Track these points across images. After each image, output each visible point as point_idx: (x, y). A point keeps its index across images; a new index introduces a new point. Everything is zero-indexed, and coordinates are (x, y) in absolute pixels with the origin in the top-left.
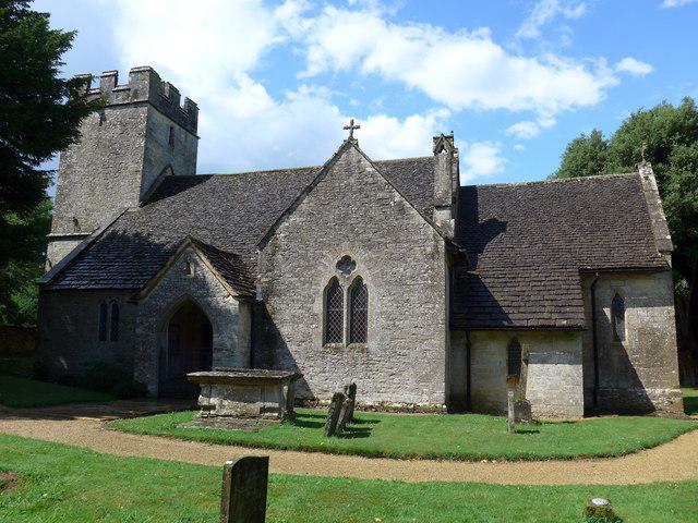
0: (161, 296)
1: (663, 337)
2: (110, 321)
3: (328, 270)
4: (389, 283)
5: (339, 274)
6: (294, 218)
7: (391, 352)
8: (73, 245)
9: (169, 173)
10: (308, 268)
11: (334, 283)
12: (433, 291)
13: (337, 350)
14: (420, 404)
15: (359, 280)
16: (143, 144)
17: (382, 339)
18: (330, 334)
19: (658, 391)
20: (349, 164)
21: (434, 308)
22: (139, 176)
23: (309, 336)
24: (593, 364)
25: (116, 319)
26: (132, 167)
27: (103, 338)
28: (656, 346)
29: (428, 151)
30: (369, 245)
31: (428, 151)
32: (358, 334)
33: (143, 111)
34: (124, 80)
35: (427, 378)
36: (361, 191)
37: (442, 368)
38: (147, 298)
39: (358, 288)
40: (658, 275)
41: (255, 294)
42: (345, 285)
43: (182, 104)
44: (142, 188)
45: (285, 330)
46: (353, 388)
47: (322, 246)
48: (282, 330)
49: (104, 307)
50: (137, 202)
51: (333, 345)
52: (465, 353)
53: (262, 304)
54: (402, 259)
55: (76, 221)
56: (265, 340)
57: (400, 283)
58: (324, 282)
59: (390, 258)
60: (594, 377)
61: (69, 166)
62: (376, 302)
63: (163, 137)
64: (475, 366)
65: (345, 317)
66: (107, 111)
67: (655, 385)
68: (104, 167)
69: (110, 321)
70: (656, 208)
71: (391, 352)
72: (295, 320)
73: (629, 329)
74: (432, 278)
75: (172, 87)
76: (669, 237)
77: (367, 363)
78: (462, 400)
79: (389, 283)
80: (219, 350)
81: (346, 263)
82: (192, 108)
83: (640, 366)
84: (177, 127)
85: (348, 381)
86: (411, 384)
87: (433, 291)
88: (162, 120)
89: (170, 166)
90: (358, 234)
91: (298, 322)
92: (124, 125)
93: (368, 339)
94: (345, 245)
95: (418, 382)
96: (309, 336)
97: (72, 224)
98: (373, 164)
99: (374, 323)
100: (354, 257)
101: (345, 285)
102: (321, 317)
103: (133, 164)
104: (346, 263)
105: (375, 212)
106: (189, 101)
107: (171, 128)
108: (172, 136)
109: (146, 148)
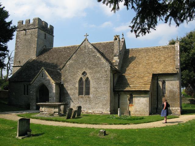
0: (36, 82)
1: (176, 93)
2: (26, 89)
3: (80, 75)
4: (95, 79)
5: (82, 76)
6: (71, 61)
7: (96, 98)
8: (19, 68)
9: (44, 47)
10: (74, 75)
11: (81, 78)
12: (107, 81)
13: (82, 97)
14: (103, 112)
15: (88, 78)
16: (37, 39)
17: (94, 94)
18: (80, 93)
19: (174, 108)
20: (85, 46)
21: (107, 86)
22: (36, 49)
23: (75, 93)
24: (156, 101)
25: (27, 89)
26: (34, 46)
27: (25, 94)
28: (174, 95)
29: (112, 40)
30: (90, 68)
31: (112, 40)
32: (88, 93)
33: (37, 29)
34: (32, 22)
35: (105, 105)
36: (88, 53)
37: (109, 102)
38: (33, 84)
39: (87, 80)
40: (175, 76)
41: (61, 82)
42: (84, 80)
43: (49, 27)
44: (36, 52)
45: (69, 92)
46: (80, 108)
47: (78, 69)
48: (68, 92)
49: (25, 86)
50: (35, 56)
51: (81, 96)
52: (118, 98)
53: (63, 85)
54: (99, 72)
55: (20, 62)
56: (63, 95)
57: (98, 79)
58: (78, 79)
59: (96, 72)
60: (157, 104)
61: (18, 47)
62: (92, 84)
63: (43, 37)
64: (121, 101)
65: (84, 88)
66: (27, 30)
67: (173, 107)
68: (27, 47)
69: (26, 89)
70: (177, 55)
71: (96, 98)
72: (71, 89)
73: (167, 91)
74: (107, 77)
75: (45, 22)
76: (179, 64)
77: (90, 101)
78: (114, 111)
79: (95, 79)
80: (50, 97)
81: (84, 73)
82: (52, 28)
83: (169, 101)
84: (47, 34)
85: (78, 105)
86: (101, 106)
87: (107, 81)
88: (42, 32)
89: (45, 45)
90: (87, 65)
91: (72, 89)
92: (31, 34)
93: (90, 94)
94: (84, 68)
95: (103, 106)
96: (75, 93)
97: (19, 63)
98: (92, 45)
99: (92, 90)
100: (86, 72)
101: (84, 80)
102: (78, 88)
103: (34, 46)
104: (84, 73)
105: (92, 59)
106: (51, 26)
107: (45, 34)
108: (45, 37)
109: (38, 41)
